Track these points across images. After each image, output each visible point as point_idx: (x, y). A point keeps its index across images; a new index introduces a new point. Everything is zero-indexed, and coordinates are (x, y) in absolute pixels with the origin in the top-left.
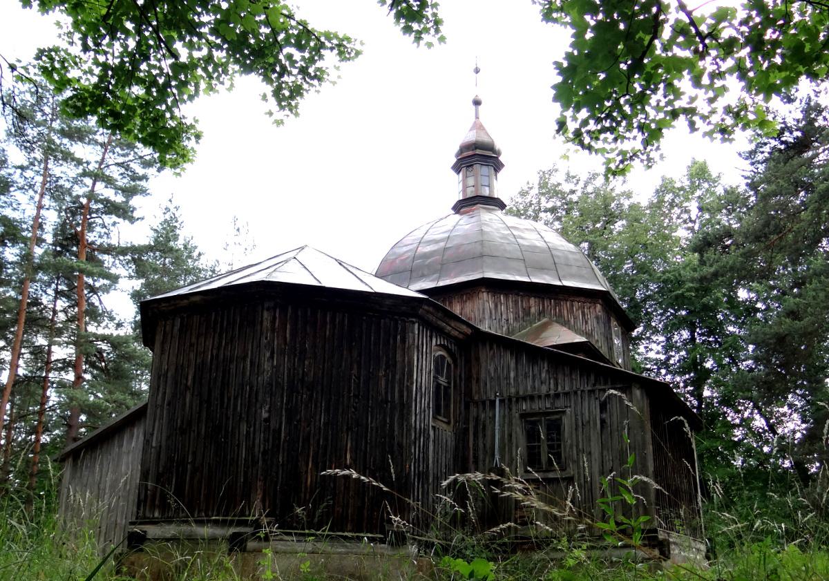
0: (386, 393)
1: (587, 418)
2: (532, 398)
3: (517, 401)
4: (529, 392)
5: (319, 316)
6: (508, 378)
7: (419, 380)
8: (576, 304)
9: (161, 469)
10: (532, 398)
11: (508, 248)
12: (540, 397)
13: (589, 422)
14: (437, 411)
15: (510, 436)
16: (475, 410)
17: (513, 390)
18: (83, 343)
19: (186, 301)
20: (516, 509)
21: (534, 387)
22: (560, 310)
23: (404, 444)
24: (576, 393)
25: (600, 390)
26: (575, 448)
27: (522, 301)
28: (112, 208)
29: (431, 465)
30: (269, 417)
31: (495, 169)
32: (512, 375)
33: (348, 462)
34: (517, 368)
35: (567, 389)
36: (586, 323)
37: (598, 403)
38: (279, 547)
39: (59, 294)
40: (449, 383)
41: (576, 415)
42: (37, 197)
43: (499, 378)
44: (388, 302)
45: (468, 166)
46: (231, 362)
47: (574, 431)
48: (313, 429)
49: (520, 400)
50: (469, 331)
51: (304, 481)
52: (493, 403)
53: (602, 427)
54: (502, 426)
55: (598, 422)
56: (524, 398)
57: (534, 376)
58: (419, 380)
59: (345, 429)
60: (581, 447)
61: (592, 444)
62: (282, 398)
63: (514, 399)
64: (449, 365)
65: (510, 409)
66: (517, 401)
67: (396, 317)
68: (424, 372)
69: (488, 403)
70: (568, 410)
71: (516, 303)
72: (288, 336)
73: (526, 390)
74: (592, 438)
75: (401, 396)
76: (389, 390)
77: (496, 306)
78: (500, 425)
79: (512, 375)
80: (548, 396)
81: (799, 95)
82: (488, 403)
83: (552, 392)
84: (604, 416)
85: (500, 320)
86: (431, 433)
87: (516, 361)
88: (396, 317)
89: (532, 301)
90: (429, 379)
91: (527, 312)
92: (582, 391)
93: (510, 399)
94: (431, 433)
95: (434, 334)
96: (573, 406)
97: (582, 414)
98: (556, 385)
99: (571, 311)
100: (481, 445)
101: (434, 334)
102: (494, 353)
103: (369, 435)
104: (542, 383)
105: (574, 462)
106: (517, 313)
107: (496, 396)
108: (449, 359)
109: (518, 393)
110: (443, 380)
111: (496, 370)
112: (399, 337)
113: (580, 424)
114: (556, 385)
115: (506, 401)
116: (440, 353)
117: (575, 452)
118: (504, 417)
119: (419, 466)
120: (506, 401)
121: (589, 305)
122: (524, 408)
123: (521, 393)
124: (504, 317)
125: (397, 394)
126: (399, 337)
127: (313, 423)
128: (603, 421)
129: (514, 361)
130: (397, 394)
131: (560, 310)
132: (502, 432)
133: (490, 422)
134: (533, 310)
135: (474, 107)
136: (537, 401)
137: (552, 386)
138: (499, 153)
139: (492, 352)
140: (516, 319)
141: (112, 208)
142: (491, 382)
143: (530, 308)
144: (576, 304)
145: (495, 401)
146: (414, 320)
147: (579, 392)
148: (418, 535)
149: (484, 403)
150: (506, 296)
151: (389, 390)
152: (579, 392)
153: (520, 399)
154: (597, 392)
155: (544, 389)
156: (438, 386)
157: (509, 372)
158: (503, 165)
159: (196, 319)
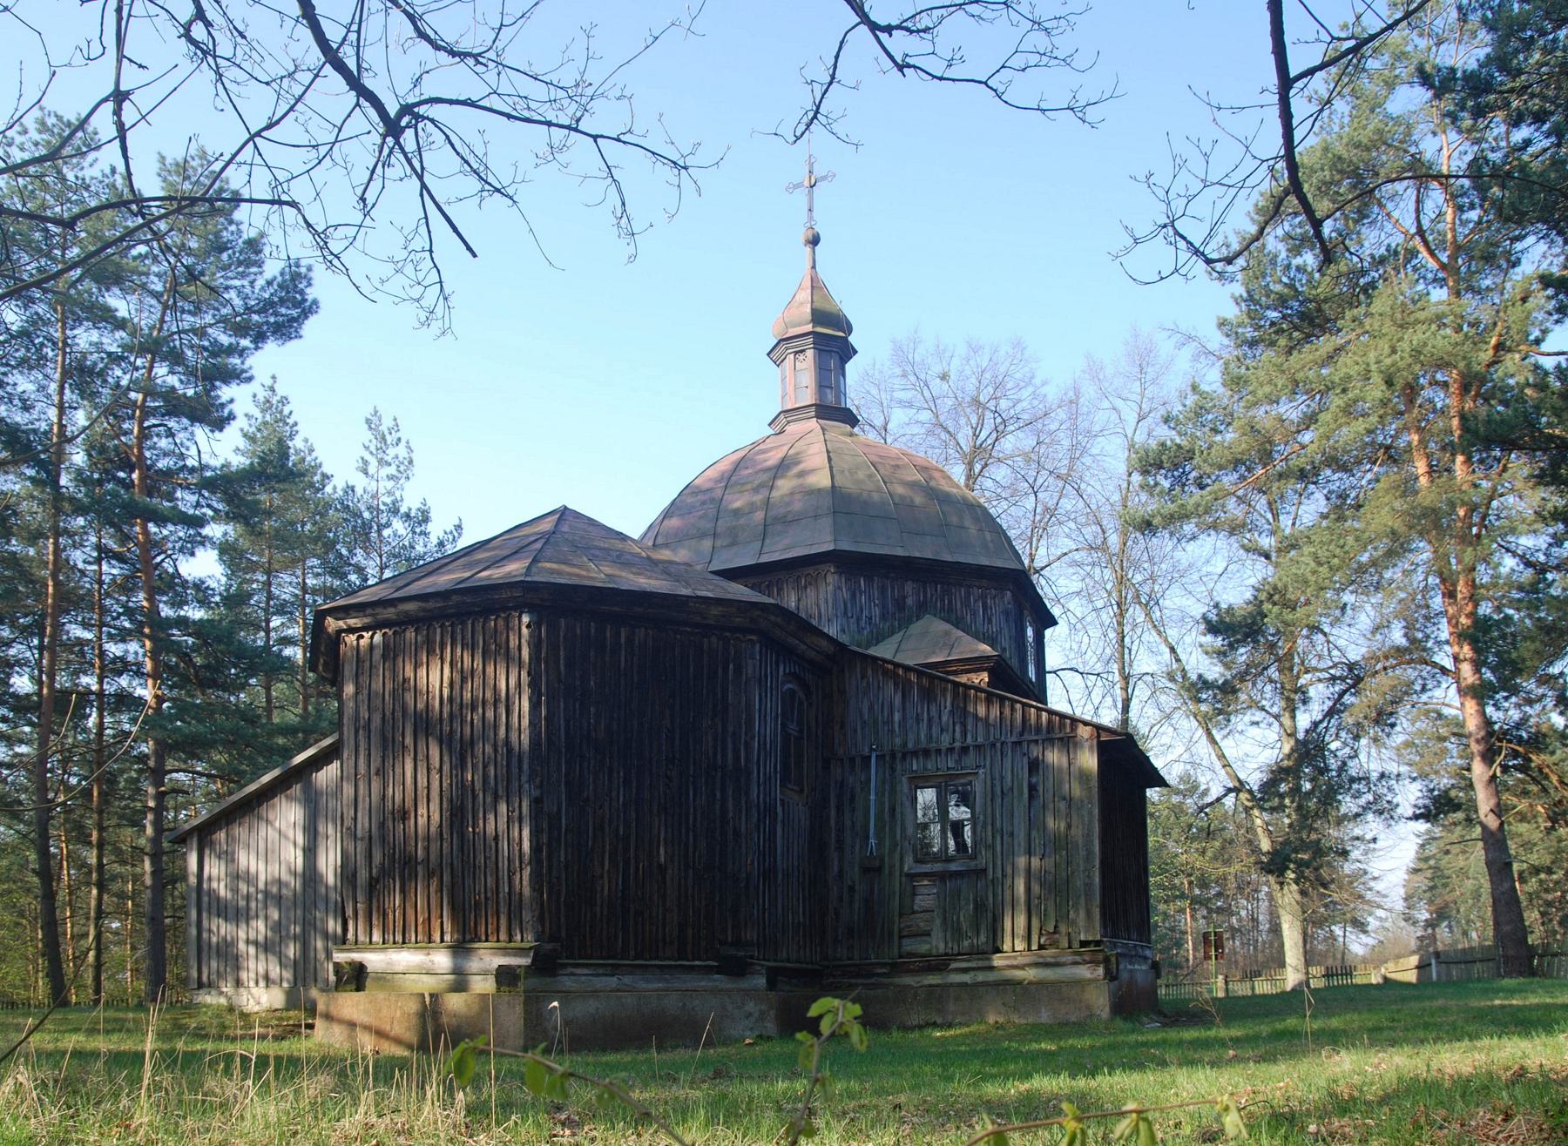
0: (715, 754)
1: (1009, 784)
2: (927, 753)
3: (904, 755)
4: (923, 745)
5: (608, 634)
6: (890, 721)
7: (762, 730)
8: (976, 592)
9: (374, 871)
10: (927, 753)
11: (876, 496)
12: (938, 751)
13: (1012, 789)
14: (785, 781)
15: (893, 810)
16: (839, 770)
17: (898, 741)
18: (154, 628)
19: (392, 610)
20: (901, 915)
21: (931, 737)
22: (950, 602)
23: (743, 830)
24: (993, 745)
25: (1030, 742)
26: (989, 827)
27: (893, 589)
28: (175, 406)
29: (779, 857)
30: (542, 794)
31: (841, 358)
32: (897, 717)
33: (662, 859)
34: (904, 709)
35: (980, 740)
36: (990, 621)
37: (1025, 760)
38: (569, 983)
39: (103, 553)
40: (801, 731)
41: (993, 779)
42: (53, 387)
43: (875, 722)
44: (715, 611)
45: (796, 353)
46: (473, 708)
47: (989, 803)
48: (607, 811)
49: (909, 756)
50: (831, 649)
51: (599, 889)
52: (866, 760)
53: (1031, 797)
54: (880, 795)
55: (1026, 790)
56: (915, 753)
57: (930, 720)
58: (762, 730)
59: (655, 811)
60: (998, 824)
61: (1016, 821)
62: (559, 764)
63: (899, 755)
64: (801, 703)
65: (893, 770)
66: (904, 755)
67: (728, 634)
68: (768, 718)
69: (858, 761)
70: (981, 771)
71: (883, 591)
72: (562, 668)
73: (918, 740)
74: (1016, 814)
75: (737, 758)
76: (719, 749)
77: (853, 596)
78: (876, 794)
79: (897, 717)
80: (951, 750)
81: (1464, 301)
82: (858, 761)
83: (957, 744)
84: (1034, 780)
85: (858, 620)
86: (779, 810)
87: (904, 696)
88: (728, 634)
89: (909, 587)
90: (776, 729)
91: (900, 604)
92: (1002, 743)
93: (893, 755)
94: (779, 810)
95: (781, 658)
96: (988, 766)
97: (1002, 778)
98: (964, 733)
99: (966, 603)
100: (848, 823)
101: (781, 658)
102: (868, 683)
103: (691, 817)
104: (942, 730)
105: (987, 847)
106: (884, 607)
107: (872, 750)
108: (801, 694)
109: (905, 744)
110: (793, 728)
111: (871, 708)
112: (731, 666)
113: (999, 793)
114: (964, 733)
115: (887, 758)
116: (789, 686)
117: (990, 834)
118: (884, 782)
119: (764, 860)
120: (887, 758)
121: (993, 591)
122: (915, 768)
123: (910, 745)
124: (866, 613)
125: (730, 755)
126: (731, 666)
127: (607, 804)
128: (1032, 788)
129: (899, 694)
130: (730, 755)
131: (950, 602)
132: (880, 803)
133: (862, 789)
134: (909, 601)
135: (808, 249)
136: (933, 758)
137: (958, 735)
138: (849, 329)
139: (865, 681)
140: (883, 617)
141: (175, 406)
142: (862, 729)
143: (905, 597)
144: (976, 592)
145: (870, 757)
146: (754, 638)
147: (998, 745)
148: (764, 960)
149: (852, 760)
150: (869, 580)
151: (719, 749)
152: (998, 745)
153: (907, 754)
154: (1025, 745)
155: (945, 740)
156: (786, 736)
157: (892, 713)
158: (855, 352)
159: (410, 634)
